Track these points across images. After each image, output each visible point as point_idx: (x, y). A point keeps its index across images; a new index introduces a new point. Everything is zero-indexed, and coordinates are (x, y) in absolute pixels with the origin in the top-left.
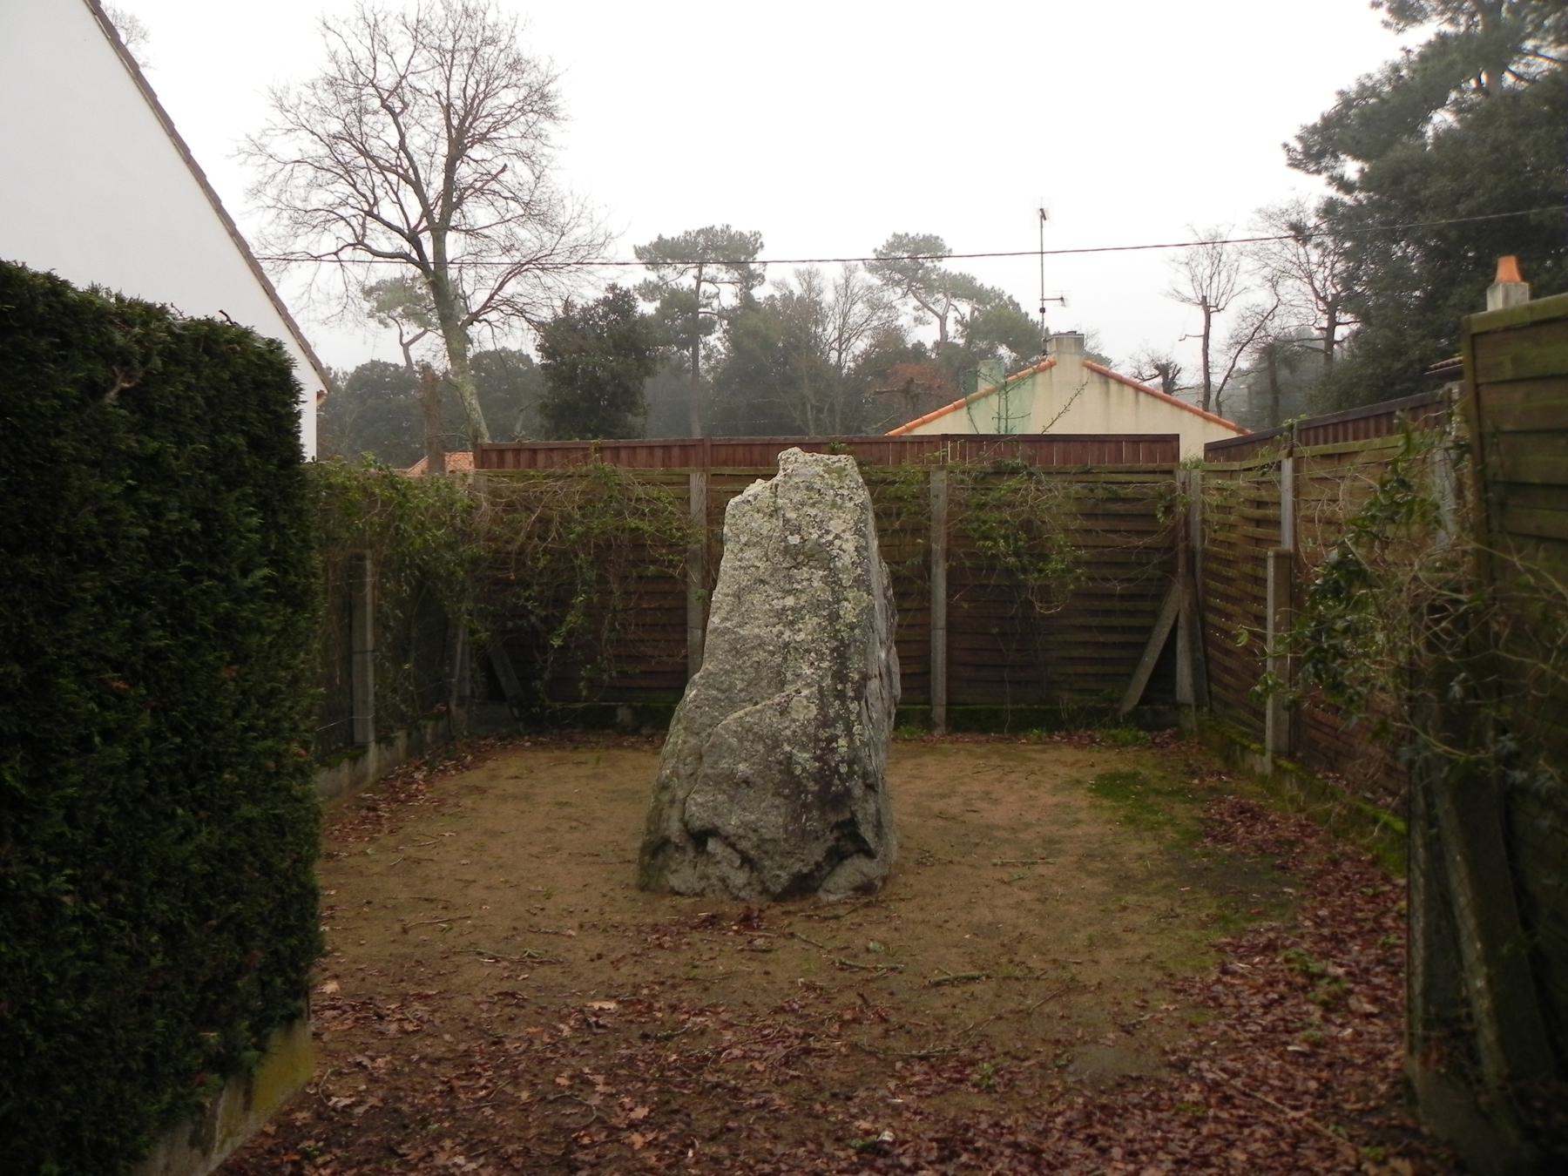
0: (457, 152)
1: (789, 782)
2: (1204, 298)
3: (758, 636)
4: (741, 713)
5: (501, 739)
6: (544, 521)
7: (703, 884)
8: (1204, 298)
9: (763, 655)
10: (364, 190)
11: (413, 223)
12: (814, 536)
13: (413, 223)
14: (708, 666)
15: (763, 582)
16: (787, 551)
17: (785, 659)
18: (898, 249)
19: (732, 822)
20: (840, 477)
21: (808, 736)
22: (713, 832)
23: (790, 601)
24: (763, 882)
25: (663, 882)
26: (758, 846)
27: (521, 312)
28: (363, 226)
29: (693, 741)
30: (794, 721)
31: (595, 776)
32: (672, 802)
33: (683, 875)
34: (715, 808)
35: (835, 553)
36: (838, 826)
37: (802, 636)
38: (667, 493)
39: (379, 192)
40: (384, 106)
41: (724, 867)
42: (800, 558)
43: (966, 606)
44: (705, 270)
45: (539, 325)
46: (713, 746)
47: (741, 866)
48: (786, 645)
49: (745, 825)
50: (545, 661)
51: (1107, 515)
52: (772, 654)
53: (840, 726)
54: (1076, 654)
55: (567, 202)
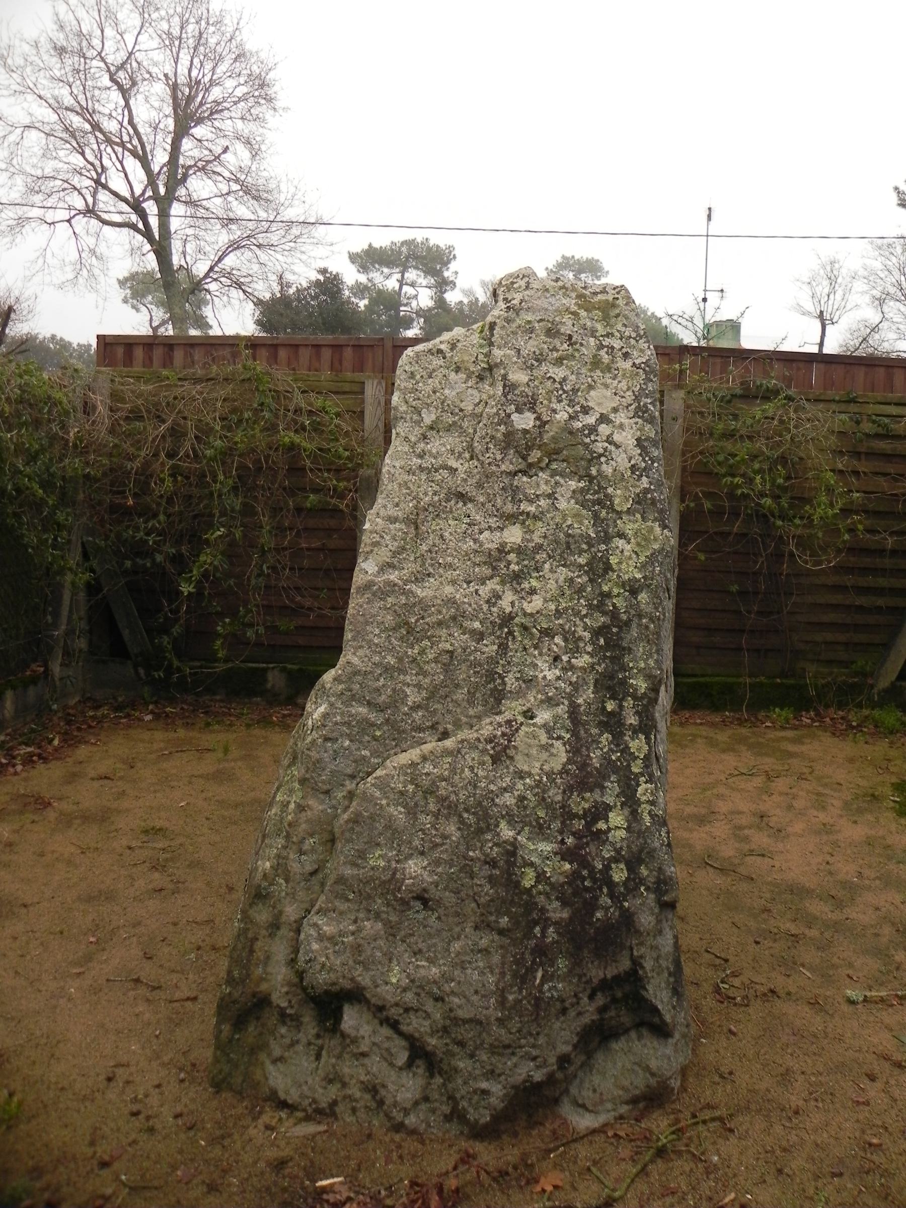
0: (181, 131)
1: (509, 900)
2: (822, 312)
3: (451, 601)
4: (414, 754)
5: (118, 709)
6: (176, 433)
7: (333, 1091)
8: (822, 312)
9: (460, 639)
10: (91, 158)
11: (138, 191)
12: (562, 416)
13: (138, 191)
14: (352, 656)
15: (462, 497)
16: (511, 441)
17: (503, 648)
18: (565, 268)
19: (393, 979)
20: (606, 318)
21: (549, 807)
22: (355, 995)
23: (514, 535)
24: (451, 1098)
25: (258, 1076)
26: (445, 1030)
27: (239, 285)
28: (94, 196)
29: (317, 806)
30: (521, 775)
31: (218, 777)
32: (275, 926)
33: (293, 1070)
34: (358, 949)
35: (599, 447)
36: (605, 985)
37: (536, 604)
38: (333, 404)
39: (106, 162)
40: (112, 80)
41: (375, 1064)
42: (535, 455)
43: (702, 557)
44: (406, 275)
45: (259, 303)
46: (356, 820)
47: (410, 1064)
48: (507, 619)
49: (419, 986)
50: (176, 611)
51: (871, 455)
52: (479, 636)
53: (612, 787)
54: (826, 618)
55: (283, 187)
